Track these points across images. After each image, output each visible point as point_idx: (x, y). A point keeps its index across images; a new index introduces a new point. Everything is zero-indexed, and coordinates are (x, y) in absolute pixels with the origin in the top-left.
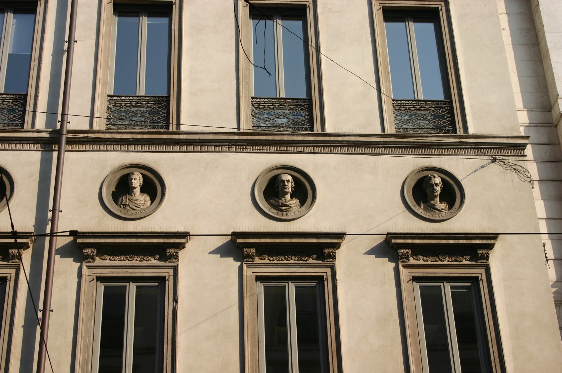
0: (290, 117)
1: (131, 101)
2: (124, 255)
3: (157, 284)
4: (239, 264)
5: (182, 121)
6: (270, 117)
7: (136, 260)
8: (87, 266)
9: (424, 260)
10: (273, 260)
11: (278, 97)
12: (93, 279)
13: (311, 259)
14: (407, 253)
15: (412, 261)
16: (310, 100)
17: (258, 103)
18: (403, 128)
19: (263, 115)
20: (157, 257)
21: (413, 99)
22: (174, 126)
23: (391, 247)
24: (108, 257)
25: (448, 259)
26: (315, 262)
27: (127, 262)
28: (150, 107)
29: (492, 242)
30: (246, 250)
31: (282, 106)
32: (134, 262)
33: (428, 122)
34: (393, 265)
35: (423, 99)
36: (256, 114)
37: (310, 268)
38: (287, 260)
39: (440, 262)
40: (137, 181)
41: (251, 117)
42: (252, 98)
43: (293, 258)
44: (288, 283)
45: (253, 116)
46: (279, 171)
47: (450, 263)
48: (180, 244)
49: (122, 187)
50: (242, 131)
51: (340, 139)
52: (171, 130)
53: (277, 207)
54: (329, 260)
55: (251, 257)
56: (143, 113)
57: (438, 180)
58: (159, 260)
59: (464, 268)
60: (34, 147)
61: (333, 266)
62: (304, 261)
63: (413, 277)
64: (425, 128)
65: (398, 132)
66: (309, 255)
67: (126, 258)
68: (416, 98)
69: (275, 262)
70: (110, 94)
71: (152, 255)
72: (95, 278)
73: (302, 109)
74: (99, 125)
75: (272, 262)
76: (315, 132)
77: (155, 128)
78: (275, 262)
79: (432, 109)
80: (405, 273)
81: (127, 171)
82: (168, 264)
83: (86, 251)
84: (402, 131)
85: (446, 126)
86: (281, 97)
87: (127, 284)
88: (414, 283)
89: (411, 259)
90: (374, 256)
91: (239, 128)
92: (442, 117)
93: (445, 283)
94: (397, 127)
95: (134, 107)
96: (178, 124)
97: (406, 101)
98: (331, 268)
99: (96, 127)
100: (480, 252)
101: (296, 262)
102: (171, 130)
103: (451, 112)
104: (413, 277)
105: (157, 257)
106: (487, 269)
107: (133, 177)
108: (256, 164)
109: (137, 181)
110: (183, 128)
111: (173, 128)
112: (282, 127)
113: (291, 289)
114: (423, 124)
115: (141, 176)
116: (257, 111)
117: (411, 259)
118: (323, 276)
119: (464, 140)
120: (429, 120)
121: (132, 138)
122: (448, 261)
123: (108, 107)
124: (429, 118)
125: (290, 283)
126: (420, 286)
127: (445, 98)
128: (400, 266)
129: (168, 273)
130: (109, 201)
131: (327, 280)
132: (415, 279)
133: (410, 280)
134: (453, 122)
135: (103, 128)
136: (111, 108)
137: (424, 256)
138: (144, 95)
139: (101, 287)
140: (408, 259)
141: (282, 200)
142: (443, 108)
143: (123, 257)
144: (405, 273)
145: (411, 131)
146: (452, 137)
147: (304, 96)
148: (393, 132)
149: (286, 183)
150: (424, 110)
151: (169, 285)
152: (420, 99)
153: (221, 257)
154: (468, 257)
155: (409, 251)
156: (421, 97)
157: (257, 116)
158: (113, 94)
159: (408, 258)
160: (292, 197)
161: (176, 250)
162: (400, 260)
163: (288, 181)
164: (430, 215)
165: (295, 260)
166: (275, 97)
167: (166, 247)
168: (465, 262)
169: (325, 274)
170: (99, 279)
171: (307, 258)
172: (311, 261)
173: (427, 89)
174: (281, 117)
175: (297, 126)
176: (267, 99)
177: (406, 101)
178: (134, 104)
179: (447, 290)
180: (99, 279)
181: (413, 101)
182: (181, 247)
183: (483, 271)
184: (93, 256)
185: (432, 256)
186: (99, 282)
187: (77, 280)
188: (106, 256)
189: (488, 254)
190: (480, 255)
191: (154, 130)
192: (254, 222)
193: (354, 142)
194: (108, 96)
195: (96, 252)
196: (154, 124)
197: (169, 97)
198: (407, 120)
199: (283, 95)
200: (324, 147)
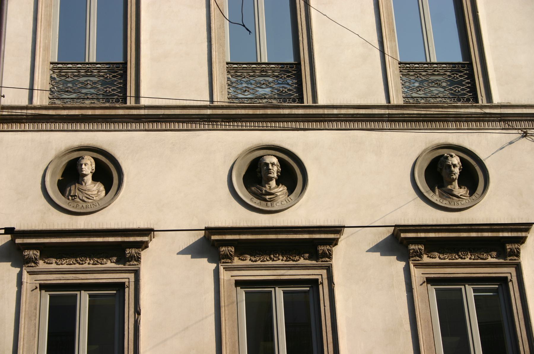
0: (275, 87)
1: (78, 70)
2: (74, 257)
3: (115, 292)
4: (214, 265)
5: (143, 93)
6: (250, 86)
7: (89, 264)
8: (28, 272)
9: (440, 258)
10: (256, 261)
11: (259, 61)
12: (36, 288)
13: (302, 259)
14: (420, 249)
15: (426, 259)
16: (298, 65)
17: (235, 69)
18: (412, 97)
19: (242, 84)
20: (114, 259)
21: (424, 61)
22: (133, 99)
23: (400, 243)
24: (54, 260)
25: (469, 256)
26: (308, 262)
27: (77, 266)
28: (103, 76)
29: (524, 234)
30: (223, 249)
31: (263, 73)
32: (279, 262)
33: (442, 90)
34: (403, 264)
35: (436, 61)
36: (232, 83)
37: (302, 270)
38: (273, 260)
39: (460, 261)
40: (88, 167)
41: (227, 87)
42: (227, 63)
43: (281, 257)
44: (275, 288)
45: (229, 85)
46: (261, 153)
47: (472, 261)
48: (142, 242)
49: (71, 175)
50: (215, 104)
51: (335, 111)
52: (128, 104)
53: (260, 196)
54: (324, 259)
55: (228, 257)
56: (95, 83)
57: (456, 160)
58: (117, 262)
59: (489, 267)
60: (8, 127)
61: (329, 267)
62: (294, 261)
63: (427, 278)
64: (439, 97)
65: (407, 102)
66: (300, 254)
67: (459, 255)
68: (428, 61)
69: (259, 263)
70: (53, 61)
71: (108, 257)
72: (38, 286)
73: (288, 76)
74: (221, 97)
75: (255, 263)
76: (305, 104)
77: (109, 102)
78: (259, 263)
79: (448, 73)
80: (417, 274)
81: (261, 153)
82: (127, 267)
83: (26, 254)
84: (411, 101)
85: (465, 94)
86: (263, 61)
87: (78, 293)
88: (429, 285)
89: (425, 256)
90: (379, 254)
91: (212, 101)
92: (460, 83)
93: (467, 286)
94: (404, 95)
95: (83, 76)
96: (138, 97)
97: (415, 64)
98: (516, 268)
99: (37, 102)
100: (508, 247)
101: (284, 262)
102: (128, 104)
103: (471, 76)
104: (427, 278)
105: (114, 259)
106: (329, 270)
107: (83, 162)
108: (236, 143)
109: (88, 167)
110: (144, 102)
111: (131, 102)
112: (265, 98)
113: (279, 296)
114: (437, 92)
115: (93, 160)
116: (234, 80)
117: (425, 256)
118: (317, 280)
119: (488, 111)
120: (443, 87)
121: (82, 115)
122: (470, 259)
123: (51, 77)
124: (444, 84)
125: (277, 288)
126: (436, 290)
127: (295, 60)
128: (412, 266)
129: (320, 274)
130: (54, 192)
131: (322, 283)
132: (430, 281)
133: (424, 282)
134: (300, 89)
135: (46, 102)
136: (54, 79)
137: (440, 253)
138: (95, 61)
139: (46, 296)
140: (421, 257)
141: (265, 187)
142: (461, 72)
143: (73, 260)
144: (417, 274)
145: (423, 101)
146: (472, 107)
147: (291, 60)
148: (401, 102)
149: (270, 167)
150: (438, 75)
151: (129, 293)
152: (432, 61)
153: (192, 258)
154: (494, 254)
155: (422, 247)
156: (434, 60)
157: (234, 85)
158: (56, 61)
159: (420, 256)
160: (278, 183)
161: (137, 250)
162: (223, 261)
163: (273, 164)
164: (447, 202)
165: (282, 260)
166: (255, 62)
167: (126, 246)
168: (490, 260)
169: (319, 277)
170: (44, 287)
171: (297, 258)
172: (302, 261)
173: (443, 50)
174: (264, 86)
175: (282, 96)
176: (418, 64)
177: (415, 64)
178: (83, 72)
179: (469, 294)
180: (44, 287)
181: (424, 64)
182: (144, 246)
183: (513, 270)
184: (36, 259)
185: (451, 253)
186: (43, 292)
187: (16, 289)
188: (51, 259)
189: (519, 249)
190: (509, 250)
191: (107, 105)
192: (232, 215)
193: (352, 115)
194: (51, 63)
195: (39, 254)
196: (107, 97)
197: (126, 63)
198: (418, 87)
199: (265, 60)
200: (316, 121)
